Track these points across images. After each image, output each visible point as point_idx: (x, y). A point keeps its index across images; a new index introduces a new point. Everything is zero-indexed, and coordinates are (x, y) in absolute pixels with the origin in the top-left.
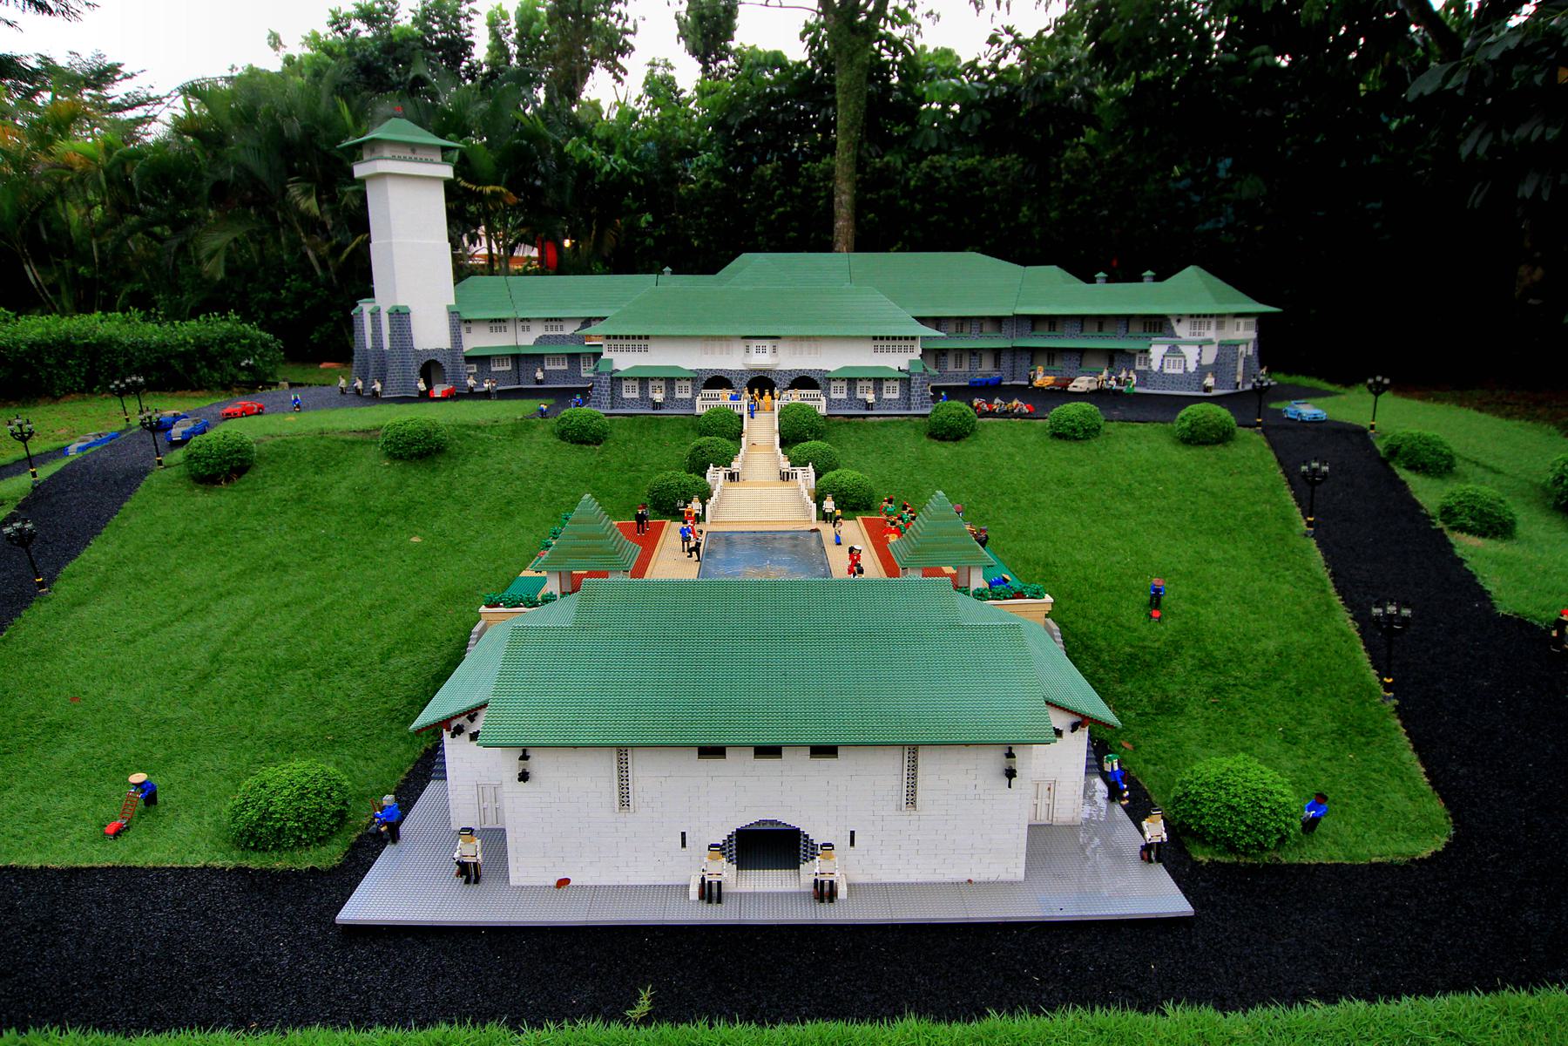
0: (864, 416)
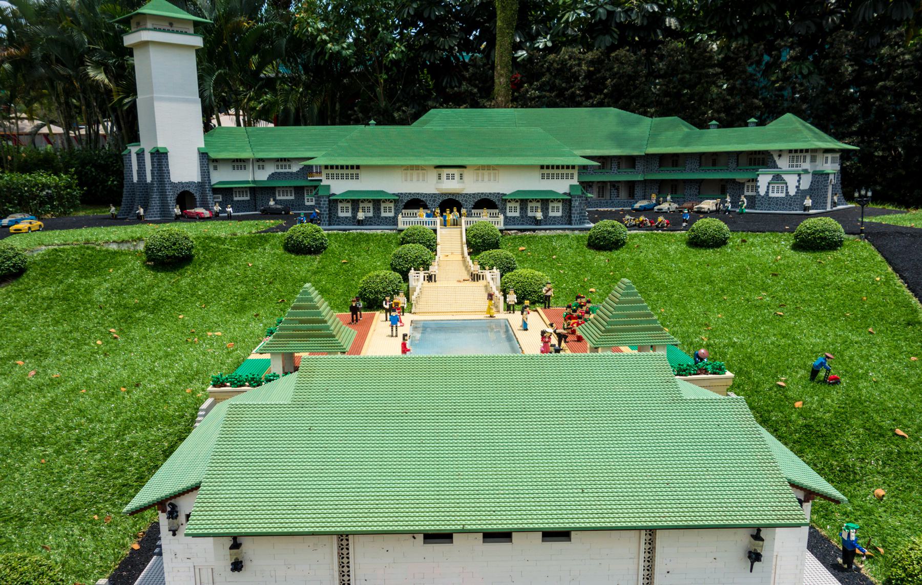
0: (534, 230)
